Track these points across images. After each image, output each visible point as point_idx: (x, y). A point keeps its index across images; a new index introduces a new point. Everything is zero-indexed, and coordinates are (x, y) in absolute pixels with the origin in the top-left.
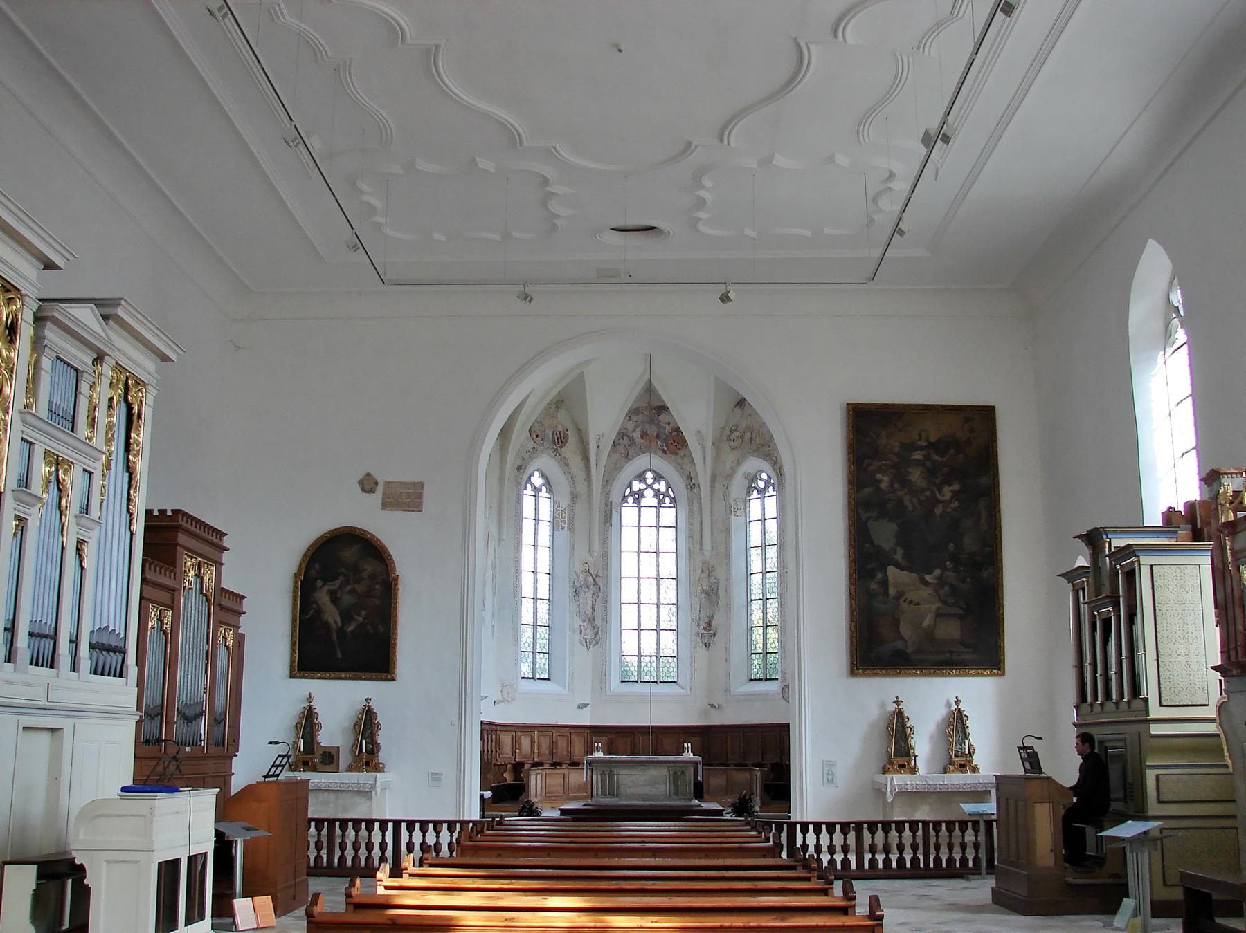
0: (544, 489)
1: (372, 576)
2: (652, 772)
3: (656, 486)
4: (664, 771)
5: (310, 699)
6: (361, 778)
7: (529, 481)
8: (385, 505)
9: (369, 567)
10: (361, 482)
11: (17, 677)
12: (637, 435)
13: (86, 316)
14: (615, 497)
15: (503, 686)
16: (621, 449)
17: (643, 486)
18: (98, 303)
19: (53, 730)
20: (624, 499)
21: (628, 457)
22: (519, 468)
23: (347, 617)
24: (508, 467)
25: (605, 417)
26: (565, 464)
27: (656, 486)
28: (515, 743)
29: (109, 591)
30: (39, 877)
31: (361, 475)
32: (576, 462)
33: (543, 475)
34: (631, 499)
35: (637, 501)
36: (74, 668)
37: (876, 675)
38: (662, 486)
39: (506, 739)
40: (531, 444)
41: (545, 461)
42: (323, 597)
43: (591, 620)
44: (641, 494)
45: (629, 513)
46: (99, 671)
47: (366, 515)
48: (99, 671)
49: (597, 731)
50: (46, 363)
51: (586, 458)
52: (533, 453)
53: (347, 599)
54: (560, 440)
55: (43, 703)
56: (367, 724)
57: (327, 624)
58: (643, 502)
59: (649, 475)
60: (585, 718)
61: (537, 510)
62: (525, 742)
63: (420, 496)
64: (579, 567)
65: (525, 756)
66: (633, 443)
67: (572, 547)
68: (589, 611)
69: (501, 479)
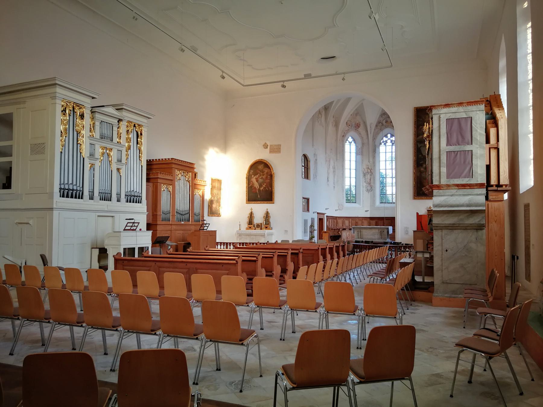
0: (353, 142)
1: (267, 173)
2: (374, 231)
3: (391, 139)
4: (377, 231)
5: (252, 209)
6: (267, 231)
7: (347, 140)
8: (270, 152)
9: (266, 170)
10: (264, 146)
11: (95, 203)
12: (384, 122)
13: (111, 110)
14: (377, 143)
15: (339, 205)
16: (379, 127)
17: (387, 139)
18: (113, 106)
19: (112, 216)
20: (381, 144)
21: (381, 130)
22: (343, 136)
23: (261, 185)
24: (339, 137)
25: (372, 119)
26: (360, 134)
27: (391, 139)
28: (343, 223)
29: (137, 182)
30: (99, 253)
31: (263, 143)
32: (363, 133)
33: (352, 138)
34: (383, 144)
35: (385, 144)
36: (119, 200)
37: (422, 199)
38: (393, 139)
39: (340, 221)
40: (347, 128)
41: (353, 133)
42: (254, 180)
43: (370, 184)
44: (386, 141)
45: (382, 148)
46: (132, 201)
47: (265, 155)
48: (132, 201)
49: (371, 218)
50: (97, 124)
51: (367, 131)
52: (348, 131)
53: (260, 180)
54: (358, 126)
55: (106, 209)
56: (267, 216)
57: (255, 188)
58: (387, 144)
59: (389, 135)
60: (368, 215)
61: (350, 149)
62: (347, 222)
63: (280, 149)
64: (365, 167)
65: (347, 227)
66: (383, 125)
67: (362, 161)
68: (369, 181)
69: (336, 140)
